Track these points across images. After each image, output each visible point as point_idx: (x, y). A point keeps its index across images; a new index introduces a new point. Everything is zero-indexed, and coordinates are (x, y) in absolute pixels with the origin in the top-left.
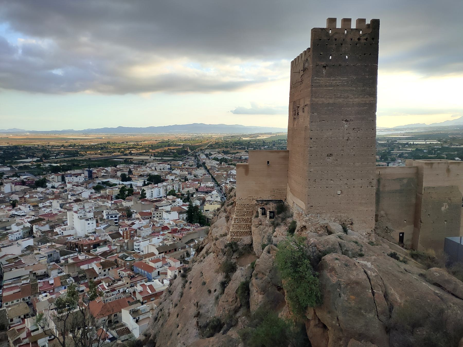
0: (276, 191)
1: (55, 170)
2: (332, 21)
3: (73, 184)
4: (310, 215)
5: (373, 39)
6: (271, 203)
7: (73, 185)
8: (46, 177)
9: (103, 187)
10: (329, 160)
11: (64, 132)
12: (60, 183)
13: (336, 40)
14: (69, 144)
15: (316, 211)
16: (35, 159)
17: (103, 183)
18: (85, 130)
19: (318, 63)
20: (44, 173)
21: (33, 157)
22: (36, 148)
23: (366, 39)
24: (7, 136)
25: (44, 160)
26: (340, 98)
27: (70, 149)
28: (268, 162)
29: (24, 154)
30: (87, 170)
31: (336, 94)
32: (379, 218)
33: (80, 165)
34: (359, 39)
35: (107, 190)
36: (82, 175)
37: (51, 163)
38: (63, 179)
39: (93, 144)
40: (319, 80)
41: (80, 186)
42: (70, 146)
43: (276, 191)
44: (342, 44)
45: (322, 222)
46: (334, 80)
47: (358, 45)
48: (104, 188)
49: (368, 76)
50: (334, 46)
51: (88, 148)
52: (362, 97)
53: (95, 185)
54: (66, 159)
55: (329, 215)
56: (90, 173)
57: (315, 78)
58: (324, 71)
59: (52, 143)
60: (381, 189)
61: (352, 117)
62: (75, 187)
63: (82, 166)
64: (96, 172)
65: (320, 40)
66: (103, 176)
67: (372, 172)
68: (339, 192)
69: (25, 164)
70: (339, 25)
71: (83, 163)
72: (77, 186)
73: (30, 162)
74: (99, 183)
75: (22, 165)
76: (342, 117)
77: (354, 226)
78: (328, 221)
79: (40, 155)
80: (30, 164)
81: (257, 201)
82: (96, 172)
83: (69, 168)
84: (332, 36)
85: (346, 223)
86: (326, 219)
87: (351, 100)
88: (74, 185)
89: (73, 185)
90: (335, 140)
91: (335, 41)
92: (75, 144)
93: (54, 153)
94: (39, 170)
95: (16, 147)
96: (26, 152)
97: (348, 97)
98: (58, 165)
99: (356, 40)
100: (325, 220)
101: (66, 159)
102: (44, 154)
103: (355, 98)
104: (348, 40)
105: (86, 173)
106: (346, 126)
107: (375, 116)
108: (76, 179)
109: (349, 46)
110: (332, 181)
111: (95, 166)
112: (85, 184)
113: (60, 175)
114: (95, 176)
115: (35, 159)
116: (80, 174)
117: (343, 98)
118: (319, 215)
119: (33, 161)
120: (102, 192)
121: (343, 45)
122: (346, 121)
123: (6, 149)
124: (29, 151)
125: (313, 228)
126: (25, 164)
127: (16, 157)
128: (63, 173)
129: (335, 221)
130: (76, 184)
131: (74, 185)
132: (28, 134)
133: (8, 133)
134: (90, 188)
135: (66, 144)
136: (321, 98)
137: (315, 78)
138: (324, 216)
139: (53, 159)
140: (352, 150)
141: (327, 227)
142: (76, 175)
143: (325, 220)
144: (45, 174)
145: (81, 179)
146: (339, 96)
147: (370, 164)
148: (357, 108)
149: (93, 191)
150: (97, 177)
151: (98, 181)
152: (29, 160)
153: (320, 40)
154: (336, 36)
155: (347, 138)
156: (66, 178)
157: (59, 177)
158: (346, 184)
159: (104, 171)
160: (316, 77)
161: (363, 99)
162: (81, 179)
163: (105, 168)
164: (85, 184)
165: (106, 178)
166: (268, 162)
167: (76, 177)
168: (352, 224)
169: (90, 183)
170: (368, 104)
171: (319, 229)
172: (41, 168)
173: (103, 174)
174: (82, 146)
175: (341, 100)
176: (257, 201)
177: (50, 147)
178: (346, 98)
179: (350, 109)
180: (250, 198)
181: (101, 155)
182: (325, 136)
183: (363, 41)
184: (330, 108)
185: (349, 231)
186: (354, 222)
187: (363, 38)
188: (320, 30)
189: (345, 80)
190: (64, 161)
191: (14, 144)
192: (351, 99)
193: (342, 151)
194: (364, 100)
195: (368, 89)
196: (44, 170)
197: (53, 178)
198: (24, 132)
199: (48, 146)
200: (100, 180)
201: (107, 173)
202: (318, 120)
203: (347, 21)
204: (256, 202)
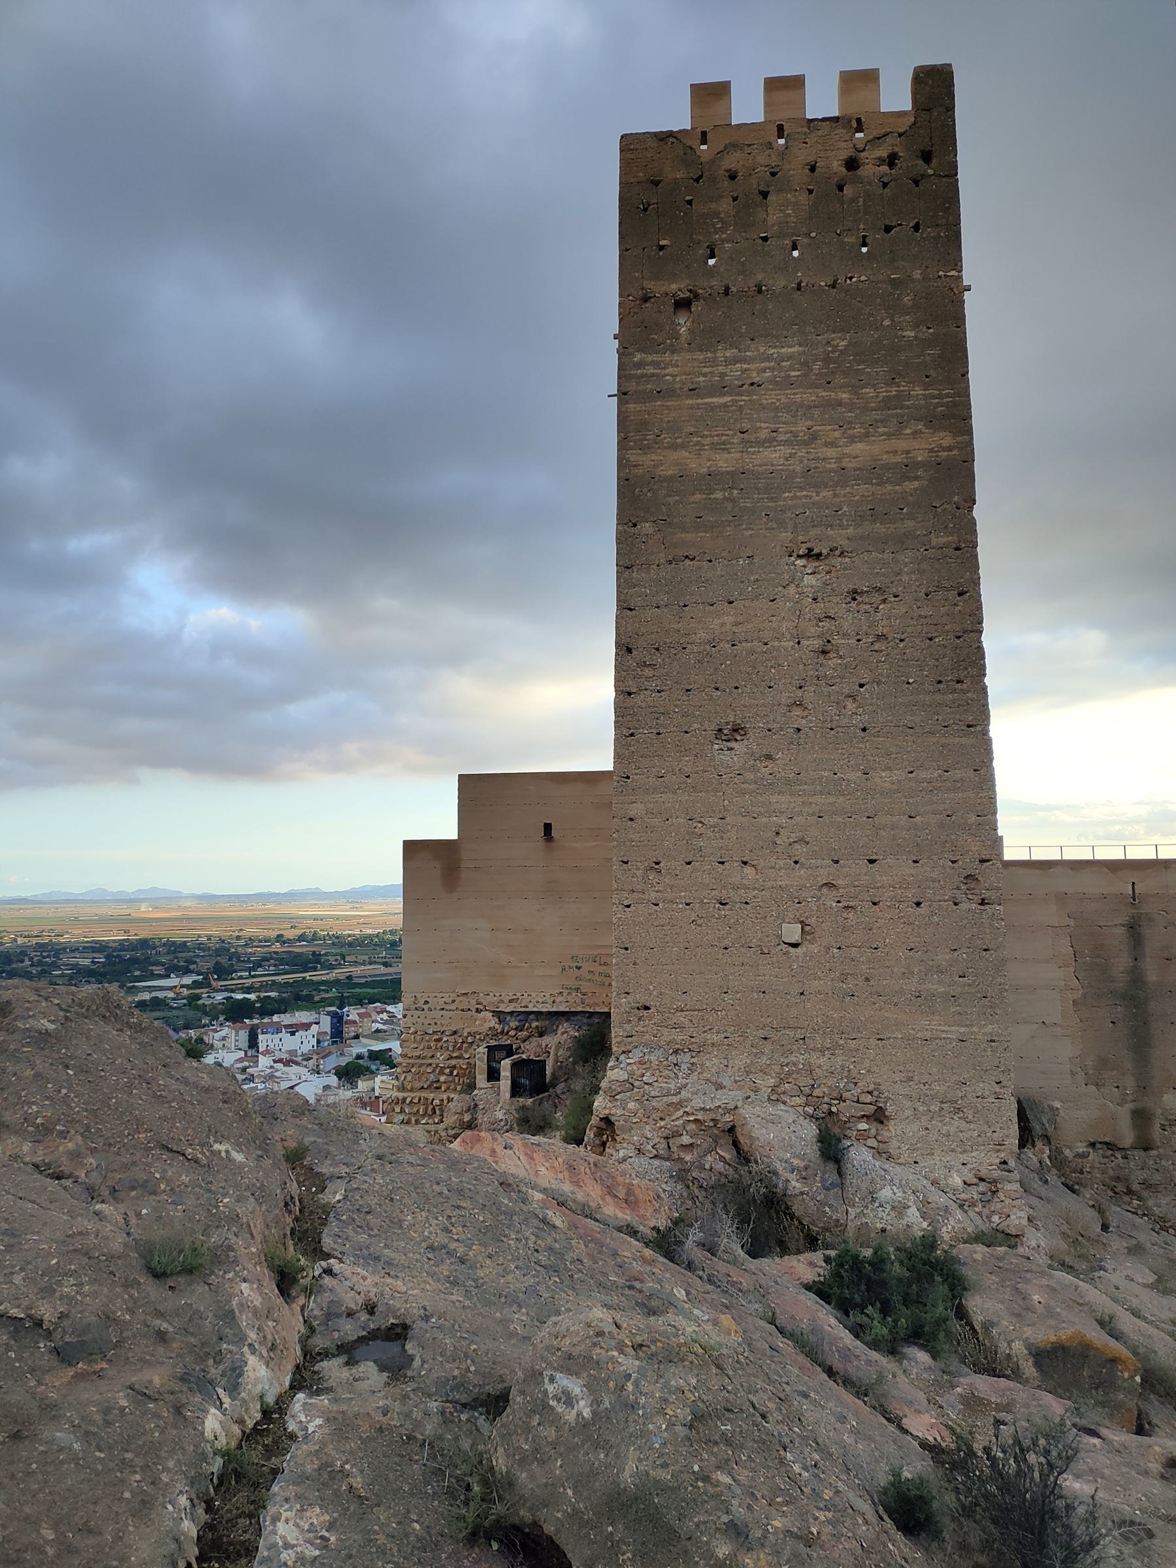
0: (586, 966)
1: (236, 1012)
2: (710, 95)
3: (278, 1055)
4: (636, 1055)
5: (927, 157)
6: (564, 1026)
7: (275, 1061)
8: (206, 1033)
9: (368, 1069)
10: (726, 757)
11: (291, 896)
12: (242, 1054)
13: (733, 177)
14: (299, 932)
15: (667, 1035)
16: (187, 980)
17: (374, 1056)
18: (353, 891)
19: (649, 285)
20: (205, 1021)
21: (187, 971)
22: (200, 947)
23: (891, 160)
24: (127, 912)
25: (214, 983)
26: (770, 442)
27: (301, 948)
28: (548, 828)
29: (163, 964)
30: (328, 1013)
31: (746, 425)
32: (1156, 1133)
33: (317, 999)
34: (852, 164)
35: (378, 1079)
36: (315, 1028)
37: (232, 991)
38: (253, 1043)
39: (369, 931)
40: (656, 364)
41: (297, 1063)
42: (302, 938)
43: (586, 966)
44: (765, 195)
45: (701, 1099)
46: (735, 361)
47: (848, 190)
48: (372, 1072)
49: (916, 326)
50: (725, 206)
51: (350, 945)
52: (889, 435)
53: (343, 1062)
54: (279, 978)
55: (740, 1060)
56: (338, 1022)
57: (638, 357)
58: (683, 322)
59: (250, 931)
60: (1152, 977)
61: (839, 536)
62: (279, 1066)
63: (322, 1000)
64: (357, 1018)
65: (656, 183)
66: (378, 1031)
67: (973, 819)
68: (793, 932)
69: (154, 994)
70: (747, 108)
71: (327, 991)
72: (287, 1063)
73: (171, 989)
74: (359, 1057)
75: (146, 996)
76: (786, 536)
77: (893, 1129)
78: (739, 1095)
79: (206, 965)
80: (171, 995)
81: (499, 1015)
82: (357, 1018)
83: (282, 1007)
84: (712, 161)
85: (846, 1110)
86: (726, 1082)
87: (830, 452)
88: (280, 1061)
89: (275, 1061)
90: (752, 652)
91: (726, 183)
92: (315, 933)
93: (249, 961)
94: (191, 1014)
95: (144, 944)
96: (170, 957)
97: (814, 437)
98: (252, 997)
99: (837, 167)
100: (720, 1087)
101: (279, 978)
102: (217, 963)
103: (852, 440)
104: (796, 170)
105: (326, 1023)
106: (809, 580)
107: (973, 522)
108: (290, 1043)
109: (803, 197)
110: (748, 870)
111: (359, 1001)
112: (315, 1057)
113: (245, 1027)
114: (349, 1031)
115: (187, 980)
116: (307, 1026)
117: (786, 443)
118: (685, 1058)
119: (182, 986)
120: (362, 1085)
121: (772, 198)
122: (810, 555)
123: (115, 950)
124: (176, 956)
125: (651, 1134)
126: (154, 994)
127: (137, 973)
128: (256, 1021)
129: (776, 1096)
130: (285, 1056)
131: (280, 1061)
132: (187, 904)
133: (133, 901)
134: (329, 1072)
135: (290, 934)
136: (674, 447)
137: (638, 357)
138: (712, 1062)
139: (241, 978)
140: (850, 705)
141: (732, 1130)
142: (293, 1030)
143: (720, 1087)
144: (204, 1026)
145: (305, 1042)
146: (764, 434)
147: (957, 774)
148: (864, 489)
149: (333, 1080)
150: (357, 1037)
151: (357, 1049)
152: (173, 981)
153: (656, 183)
154: (733, 161)
155: (817, 643)
156: (261, 1037)
157: (242, 1033)
158: (830, 885)
159: (385, 1016)
160: (642, 350)
161: (895, 443)
162: (305, 1042)
163: (389, 1008)
164: (312, 1061)
165: (383, 1040)
166: (548, 828)
167: (293, 1034)
168: (879, 1117)
169: (329, 1054)
170: (922, 465)
171: (686, 1140)
172: (197, 1008)
173: (376, 1026)
174: (337, 938)
175: (775, 455)
176: (499, 1015)
177: (242, 942)
178: (805, 443)
179: (825, 493)
180: (464, 1003)
181: (386, 965)
182: (702, 635)
183: (870, 170)
184: (719, 495)
185: (859, 1155)
186: (890, 1109)
187: (869, 156)
188: (652, 143)
189: (790, 357)
190: (274, 985)
191: (143, 934)
192: (832, 444)
193: (797, 712)
194: (901, 444)
195: (918, 391)
196: (206, 1014)
197: (224, 1039)
198: (177, 897)
199: (238, 938)
200: (365, 1046)
201: (392, 1023)
202: (662, 557)
203: (784, 88)
204: (493, 1022)
